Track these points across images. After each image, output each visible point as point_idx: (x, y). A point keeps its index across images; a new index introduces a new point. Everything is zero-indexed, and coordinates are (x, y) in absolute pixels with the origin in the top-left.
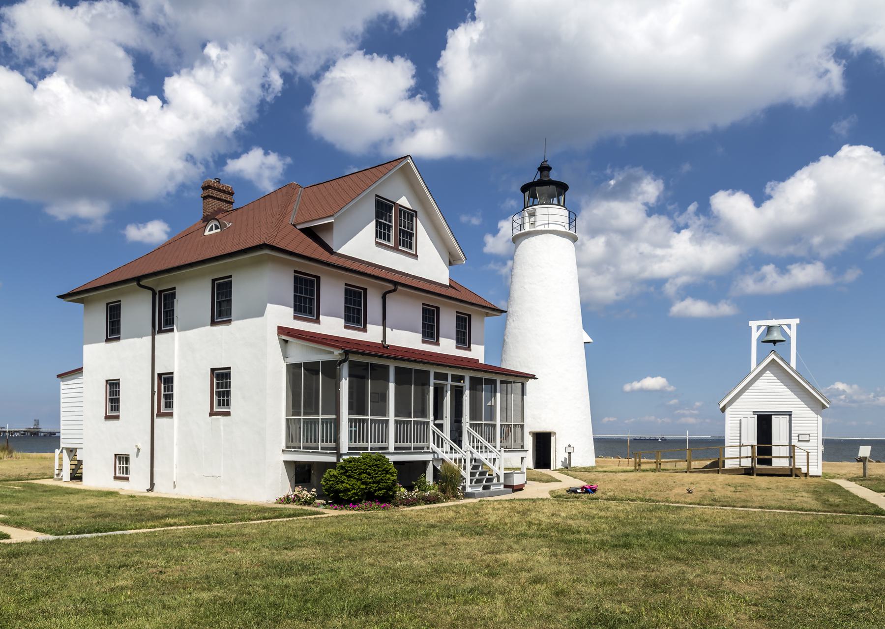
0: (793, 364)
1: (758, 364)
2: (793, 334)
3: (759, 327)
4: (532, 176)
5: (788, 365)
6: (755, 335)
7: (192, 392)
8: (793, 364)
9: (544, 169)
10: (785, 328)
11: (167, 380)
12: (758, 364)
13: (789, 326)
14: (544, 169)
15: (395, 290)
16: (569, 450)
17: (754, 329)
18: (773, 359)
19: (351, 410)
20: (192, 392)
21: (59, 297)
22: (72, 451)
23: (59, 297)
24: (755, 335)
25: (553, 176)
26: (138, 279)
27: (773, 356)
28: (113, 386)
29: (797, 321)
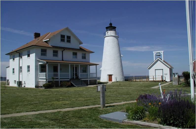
0: (163, 60)
1: (155, 60)
2: (162, 54)
3: (155, 53)
4: (108, 25)
5: (162, 59)
6: (154, 54)
7: (25, 69)
8: (163, 60)
9: (111, 24)
10: (161, 53)
11: (21, 68)
12: (155, 60)
13: (161, 52)
14: (111, 24)
15: (64, 50)
16: (116, 78)
17: (154, 53)
18: (158, 59)
19: (75, 72)
20: (25, 69)
21: (6, 54)
22: (8, 80)
23: (6, 54)
24: (154, 54)
25: (113, 25)
26: (16, 51)
27: (158, 58)
28: (13, 69)
29: (163, 51)
